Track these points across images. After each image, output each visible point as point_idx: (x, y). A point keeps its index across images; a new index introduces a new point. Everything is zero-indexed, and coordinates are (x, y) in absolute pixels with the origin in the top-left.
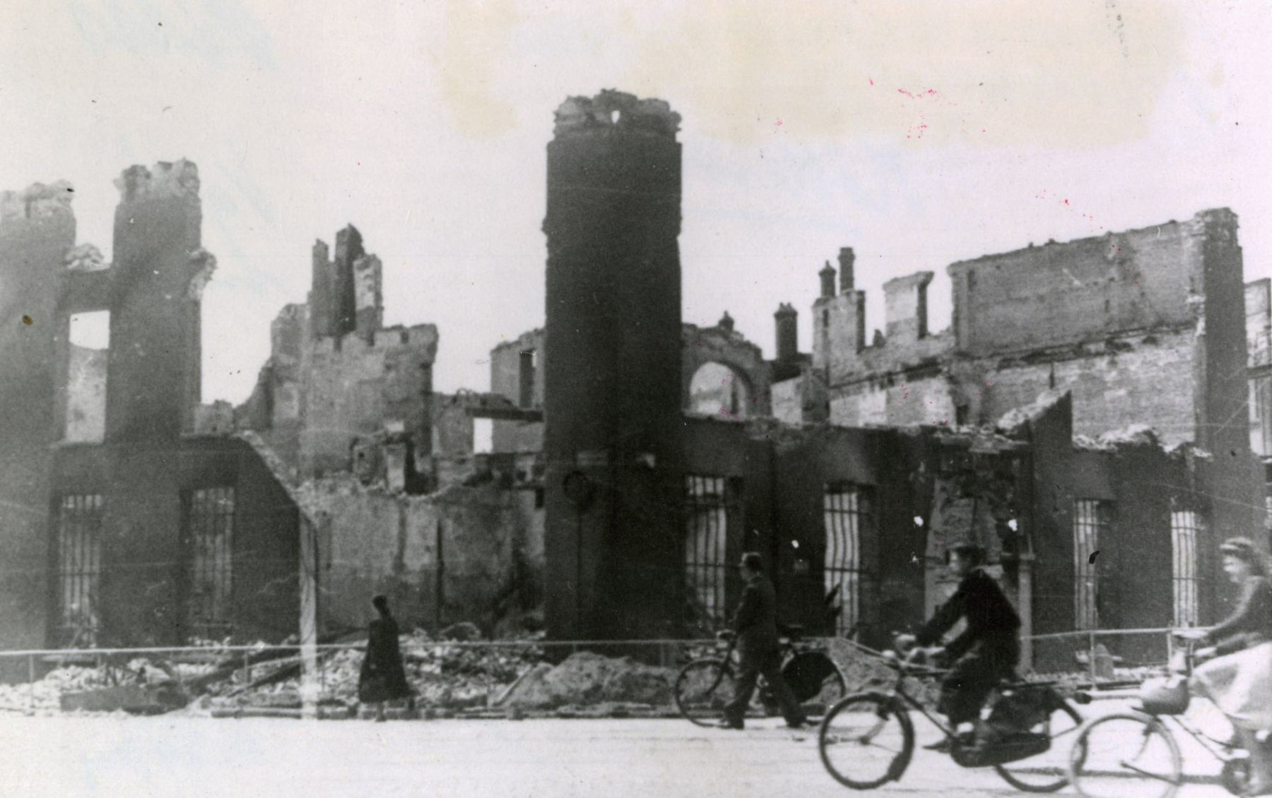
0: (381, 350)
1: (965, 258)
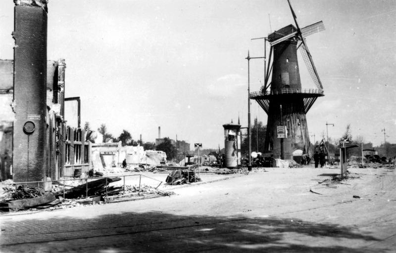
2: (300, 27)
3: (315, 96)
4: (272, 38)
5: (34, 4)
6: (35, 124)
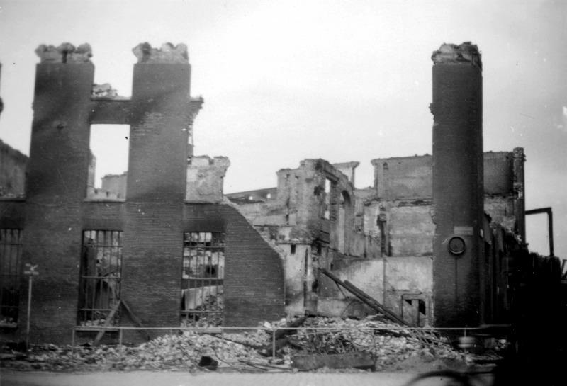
0: (196, 167)
1: (382, 157)
5: (460, 58)
6: (465, 240)
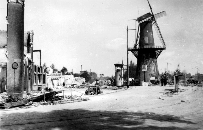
2: (154, 14)
3: (161, 49)
4: (139, 19)
5: (17, 2)
6: (18, 64)
